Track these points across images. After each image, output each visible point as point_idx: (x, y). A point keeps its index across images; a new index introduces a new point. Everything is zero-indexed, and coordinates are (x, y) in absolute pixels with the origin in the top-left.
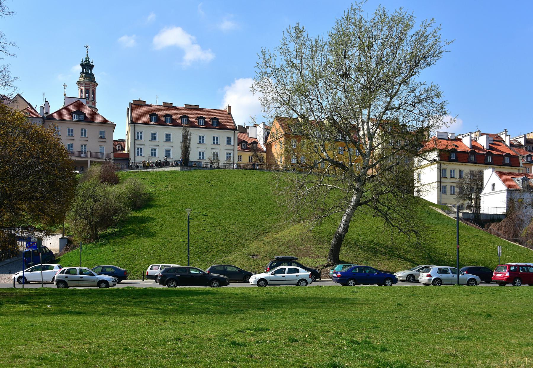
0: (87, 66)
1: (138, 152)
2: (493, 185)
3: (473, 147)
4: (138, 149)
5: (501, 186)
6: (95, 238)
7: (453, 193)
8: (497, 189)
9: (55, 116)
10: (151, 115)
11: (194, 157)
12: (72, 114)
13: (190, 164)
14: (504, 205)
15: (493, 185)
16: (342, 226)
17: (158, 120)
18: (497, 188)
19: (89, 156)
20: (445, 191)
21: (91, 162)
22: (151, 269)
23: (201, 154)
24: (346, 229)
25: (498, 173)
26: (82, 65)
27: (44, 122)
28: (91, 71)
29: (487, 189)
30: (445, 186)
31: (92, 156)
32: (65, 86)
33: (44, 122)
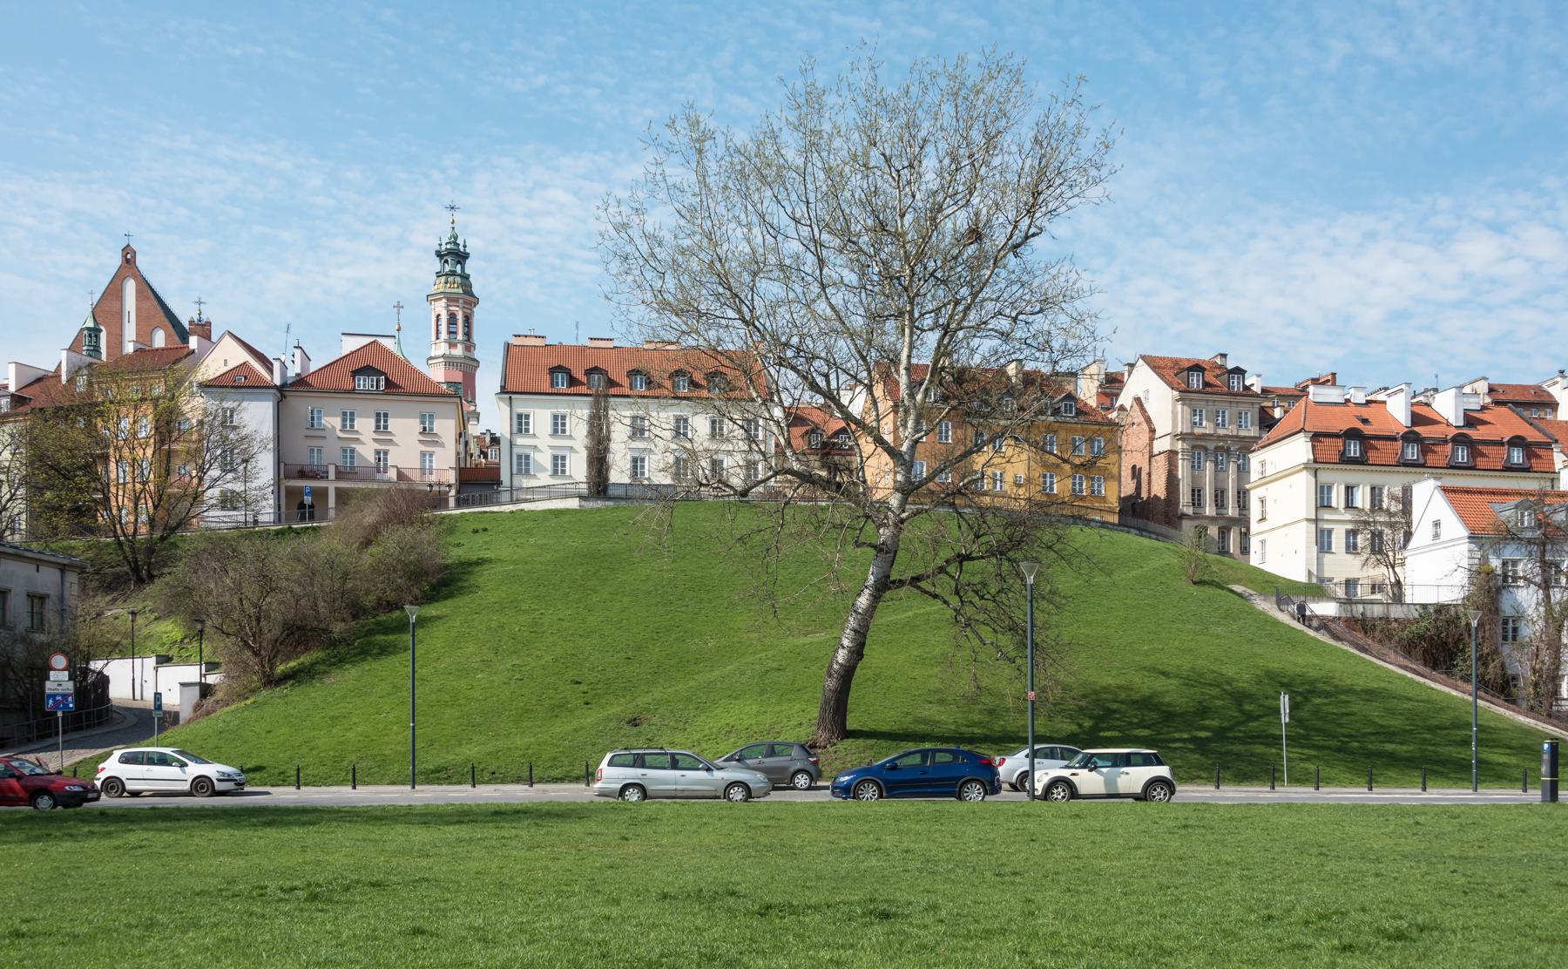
0: (455, 255)
1: (519, 464)
2: (1437, 524)
3: (1417, 419)
4: (519, 457)
5: (1455, 529)
6: (272, 681)
7: (1351, 548)
8: (1443, 538)
9: (310, 380)
10: (553, 371)
11: (619, 474)
12: (355, 373)
13: (611, 492)
14: (1461, 578)
15: (1437, 524)
16: (846, 642)
17: (573, 382)
18: (1445, 533)
19: (332, 475)
20: (1330, 544)
21: (339, 492)
22: (610, 764)
23: (637, 463)
24: (858, 652)
25: (1445, 490)
26: (439, 254)
27: (283, 396)
28: (463, 269)
29: (1422, 533)
30: (1330, 532)
31: (340, 475)
32: (399, 306)
33: (283, 396)
